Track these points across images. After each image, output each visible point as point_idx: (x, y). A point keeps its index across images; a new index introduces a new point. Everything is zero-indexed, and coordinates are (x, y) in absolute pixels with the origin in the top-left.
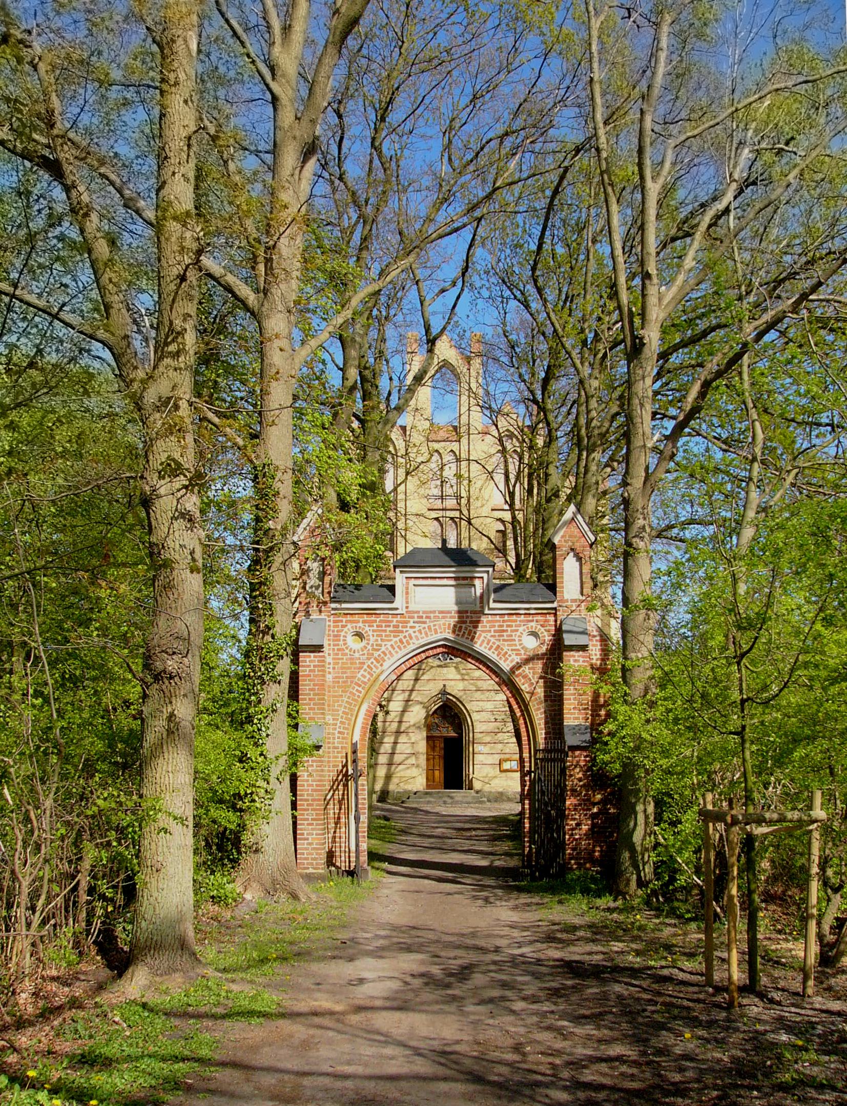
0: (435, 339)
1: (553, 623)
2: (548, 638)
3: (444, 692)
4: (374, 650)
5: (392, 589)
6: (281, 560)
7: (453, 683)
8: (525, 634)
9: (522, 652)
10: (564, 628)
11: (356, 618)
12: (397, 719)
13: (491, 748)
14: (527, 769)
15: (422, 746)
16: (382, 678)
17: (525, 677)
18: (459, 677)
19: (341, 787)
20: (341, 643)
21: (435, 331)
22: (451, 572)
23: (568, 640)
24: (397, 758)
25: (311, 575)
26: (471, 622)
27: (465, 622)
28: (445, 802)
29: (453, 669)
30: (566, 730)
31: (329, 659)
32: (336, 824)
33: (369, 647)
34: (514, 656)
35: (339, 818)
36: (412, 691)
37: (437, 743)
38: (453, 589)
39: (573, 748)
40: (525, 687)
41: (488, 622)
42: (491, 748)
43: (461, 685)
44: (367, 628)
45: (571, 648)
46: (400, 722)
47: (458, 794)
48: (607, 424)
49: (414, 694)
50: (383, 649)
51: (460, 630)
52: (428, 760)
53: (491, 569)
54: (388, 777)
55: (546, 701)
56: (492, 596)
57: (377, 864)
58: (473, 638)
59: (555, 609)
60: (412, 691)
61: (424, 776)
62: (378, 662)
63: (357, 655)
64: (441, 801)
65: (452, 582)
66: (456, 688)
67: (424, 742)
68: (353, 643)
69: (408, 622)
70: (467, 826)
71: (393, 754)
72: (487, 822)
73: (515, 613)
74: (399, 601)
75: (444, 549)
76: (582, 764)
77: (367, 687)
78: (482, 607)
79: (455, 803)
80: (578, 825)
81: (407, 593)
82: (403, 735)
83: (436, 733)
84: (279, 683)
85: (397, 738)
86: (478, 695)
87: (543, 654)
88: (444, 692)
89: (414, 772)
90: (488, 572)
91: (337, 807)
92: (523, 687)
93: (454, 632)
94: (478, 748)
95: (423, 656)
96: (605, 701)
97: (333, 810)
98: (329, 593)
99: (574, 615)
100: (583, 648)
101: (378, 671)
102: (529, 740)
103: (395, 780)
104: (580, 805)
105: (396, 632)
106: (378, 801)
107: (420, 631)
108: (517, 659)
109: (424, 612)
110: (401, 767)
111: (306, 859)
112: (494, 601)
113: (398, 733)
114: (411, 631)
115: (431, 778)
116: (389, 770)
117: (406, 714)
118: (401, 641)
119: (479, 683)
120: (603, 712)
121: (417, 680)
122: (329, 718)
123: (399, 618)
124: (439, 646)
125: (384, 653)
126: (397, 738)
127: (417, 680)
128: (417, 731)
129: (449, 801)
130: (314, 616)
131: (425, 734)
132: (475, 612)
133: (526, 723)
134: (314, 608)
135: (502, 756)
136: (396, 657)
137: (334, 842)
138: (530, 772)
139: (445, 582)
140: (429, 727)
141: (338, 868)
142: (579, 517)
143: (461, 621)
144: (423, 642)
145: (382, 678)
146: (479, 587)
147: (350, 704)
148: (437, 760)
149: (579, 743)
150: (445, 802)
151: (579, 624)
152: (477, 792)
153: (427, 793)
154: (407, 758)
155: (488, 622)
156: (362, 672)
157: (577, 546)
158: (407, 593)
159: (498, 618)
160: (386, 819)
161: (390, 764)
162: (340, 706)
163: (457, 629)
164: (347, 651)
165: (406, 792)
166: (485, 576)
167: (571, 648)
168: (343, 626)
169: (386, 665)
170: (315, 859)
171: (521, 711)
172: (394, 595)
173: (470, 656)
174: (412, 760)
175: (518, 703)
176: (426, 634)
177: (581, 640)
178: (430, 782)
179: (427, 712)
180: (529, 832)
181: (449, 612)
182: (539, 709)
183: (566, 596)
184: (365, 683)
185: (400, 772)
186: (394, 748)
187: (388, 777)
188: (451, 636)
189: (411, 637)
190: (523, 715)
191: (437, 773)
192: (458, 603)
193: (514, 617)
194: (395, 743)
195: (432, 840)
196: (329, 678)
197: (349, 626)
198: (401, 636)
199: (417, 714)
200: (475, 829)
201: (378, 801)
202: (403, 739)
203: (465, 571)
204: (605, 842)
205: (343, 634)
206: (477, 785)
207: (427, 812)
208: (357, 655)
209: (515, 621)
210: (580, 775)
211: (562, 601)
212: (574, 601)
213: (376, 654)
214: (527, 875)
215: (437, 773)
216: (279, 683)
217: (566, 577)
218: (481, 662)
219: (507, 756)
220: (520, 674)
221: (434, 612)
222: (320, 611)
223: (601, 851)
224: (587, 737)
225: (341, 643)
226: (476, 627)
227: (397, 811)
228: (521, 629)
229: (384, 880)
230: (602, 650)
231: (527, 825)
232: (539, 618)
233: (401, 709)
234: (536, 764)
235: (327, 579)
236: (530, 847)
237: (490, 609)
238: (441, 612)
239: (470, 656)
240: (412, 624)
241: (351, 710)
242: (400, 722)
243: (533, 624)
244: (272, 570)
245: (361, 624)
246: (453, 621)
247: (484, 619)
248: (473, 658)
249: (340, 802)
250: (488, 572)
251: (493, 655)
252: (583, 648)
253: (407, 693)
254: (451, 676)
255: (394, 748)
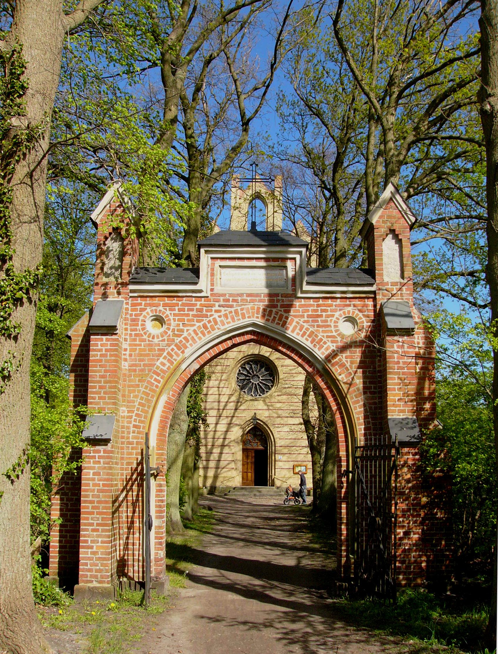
0: (249, 120)
1: (371, 308)
2: (366, 323)
3: (254, 418)
4: (175, 335)
5: (196, 272)
6: (26, 170)
7: (261, 412)
8: (341, 320)
9: (339, 339)
10: (386, 311)
11: (156, 301)
12: (222, 437)
13: (289, 458)
14: (344, 469)
15: (239, 455)
16: (184, 366)
17: (343, 365)
18: (265, 407)
19: (135, 488)
20: (140, 327)
21: (248, 115)
22: (261, 252)
23: (392, 323)
24: (222, 464)
25: (111, 256)
26: (282, 306)
27: (275, 306)
28: (255, 495)
29: (261, 402)
30: (391, 424)
31: (125, 345)
32: (129, 528)
33: (170, 332)
34: (329, 344)
35: (132, 522)
36: (233, 417)
37: (250, 454)
38: (262, 272)
39: (403, 444)
40: (342, 377)
41: (301, 306)
42: (289, 458)
43: (267, 413)
44: (168, 312)
45: (393, 332)
46: (225, 439)
47: (264, 489)
48: (404, 152)
49: (234, 419)
50: (185, 334)
51: (270, 314)
52: (243, 465)
53: (304, 250)
54: (216, 477)
55: (365, 393)
56: (306, 278)
57: (183, 565)
58: (285, 323)
59: (374, 293)
60: (233, 417)
61: (241, 476)
62: (179, 348)
63: (156, 341)
64: (252, 494)
65: (263, 263)
66: (263, 415)
67: (241, 452)
68: (152, 328)
69: (214, 305)
70: (272, 515)
71: (219, 461)
72: (286, 512)
73: (330, 296)
74: (203, 283)
75: (253, 230)
76: (410, 462)
77: (167, 376)
78: (295, 290)
79: (262, 496)
80: (407, 534)
81: (212, 275)
82: (227, 447)
83: (249, 447)
84: (16, 338)
85: (222, 450)
86: (278, 421)
87: (362, 342)
88: (254, 418)
89: (234, 473)
90: (300, 253)
91: (130, 509)
92: (340, 378)
93: (263, 316)
94: (278, 457)
95: (229, 343)
96: (430, 394)
97: (125, 513)
98: (129, 273)
99: (394, 299)
100: (408, 332)
101: (179, 359)
102: (346, 437)
103: (220, 479)
104: (409, 510)
105: (200, 316)
106: (208, 494)
107: (226, 316)
108: (333, 347)
109: (231, 295)
110: (225, 470)
111: (90, 570)
112: (308, 283)
113: (223, 446)
114: (216, 315)
115: (245, 477)
116: (216, 472)
117: (229, 433)
118: (205, 326)
119: (280, 412)
120: (427, 406)
121: (236, 409)
122: (123, 411)
123: (203, 301)
124: (247, 333)
125: (186, 338)
126: (222, 450)
127: (236, 409)
128: (235, 444)
129: (258, 494)
130: (113, 297)
131: (241, 447)
132: (286, 296)
133: (342, 418)
134: (112, 291)
135: (296, 463)
136: (199, 343)
137: (126, 549)
138: (347, 472)
139: (254, 263)
140: (244, 442)
141: (130, 579)
142: (398, 197)
143: (272, 305)
144: (228, 327)
145: (184, 366)
146: (291, 269)
147: (147, 394)
148: (249, 466)
149: (407, 439)
150: (255, 495)
151: (400, 307)
152: (278, 488)
153: (242, 489)
154: (228, 464)
155: (301, 306)
156: (161, 359)
157: (396, 227)
158: (212, 275)
159: (311, 302)
160: (210, 509)
161: (217, 468)
162: (136, 396)
163: (267, 313)
164: (145, 337)
165: (228, 487)
166: (298, 257)
167: (393, 332)
168: (142, 310)
169: (188, 352)
170: (100, 571)
171: (338, 404)
172: (198, 277)
173: (281, 343)
174: (232, 465)
175: (333, 396)
176: (233, 319)
177: (406, 323)
178: (244, 479)
179: (244, 431)
180: (347, 540)
181: (258, 295)
182: (358, 402)
183: (386, 279)
184: (164, 372)
185: (224, 474)
186: (220, 457)
187: (216, 477)
188: (260, 321)
189: (216, 322)
190: (339, 409)
191: (249, 474)
192: (269, 285)
193: (330, 302)
194: (221, 453)
195: (243, 530)
196: (125, 365)
197: (149, 310)
198: (205, 321)
199: (236, 433)
200: (278, 519)
201: (208, 494)
202: (226, 450)
203: (276, 251)
204: (432, 551)
205: (141, 318)
206: (278, 483)
207: (242, 502)
208: (156, 341)
209: (331, 305)
210: (409, 476)
211: (383, 283)
212: (394, 284)
213: (177, 340)
214: (346, 589)
215: (249, 474)
216: (16, 338)
217: (385, 260)
218: (293, 350)
219: (300, 463)
220: (337, 363)
221: (241, 295)
222: (119, 293)
223: (427, 562)
224: (416, 432)
225: (140, 327)
226: (289, 311)
227: (222, 502)
228: (337, 314)
229: (184, 592)
230: (426, 338)
231: (344, 532)
232: (357, 302)
233: (225, 430)
234: (355, 463)
235: (127, 259)
236: (347, 556)
237: (303, 292)
238: (249, 295)
239: (281, 343)
240: (217, 308)
241: (148, 401)
242: (225, 439)
243: (350, 309)
244: (13, 182)
245: (161, 308)
246: (262, 304)
247: (297, 303)
248: (285, 345)
249: (134, 505)
250: (300, 253)
251: (307, 343)
252: (408, 332)
253: (230, 418)
254: (260, 407)
255: (220, 457)
